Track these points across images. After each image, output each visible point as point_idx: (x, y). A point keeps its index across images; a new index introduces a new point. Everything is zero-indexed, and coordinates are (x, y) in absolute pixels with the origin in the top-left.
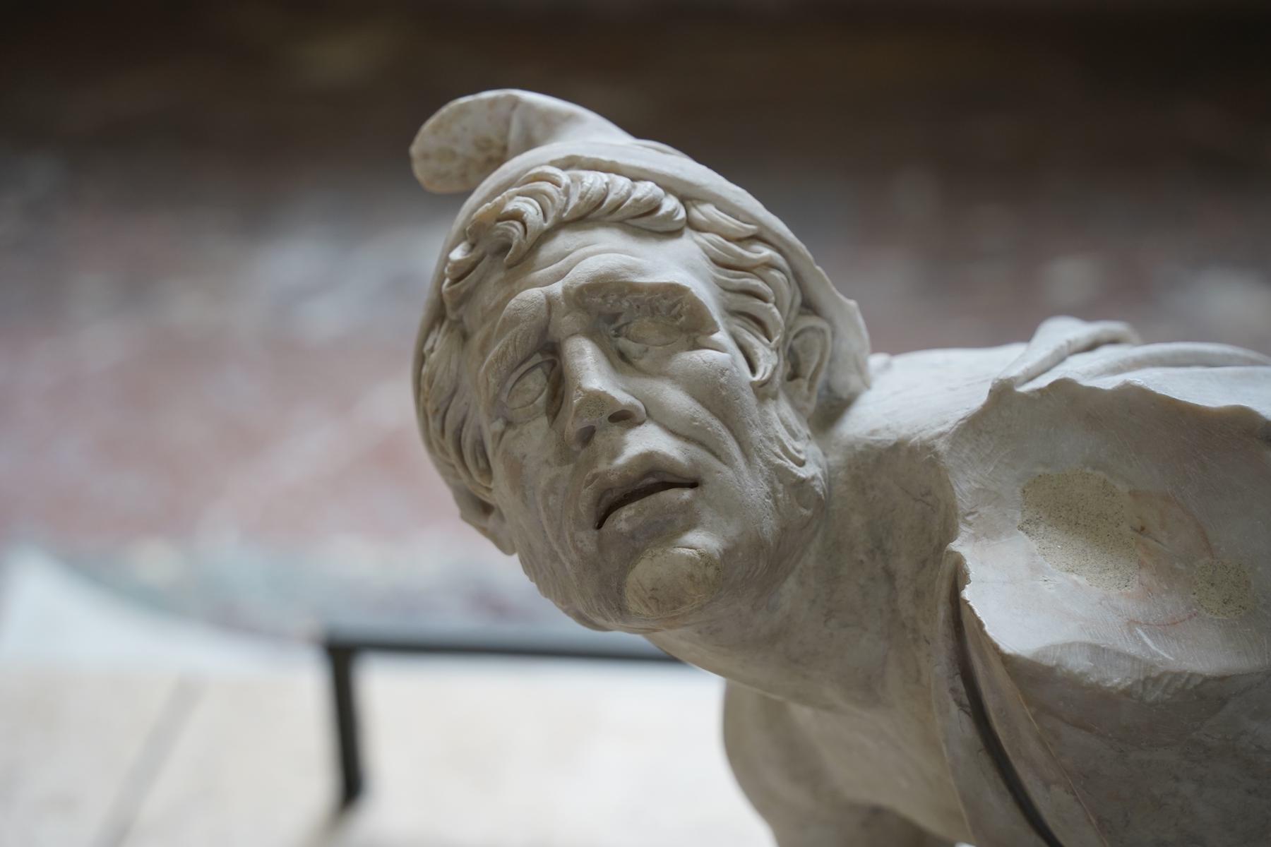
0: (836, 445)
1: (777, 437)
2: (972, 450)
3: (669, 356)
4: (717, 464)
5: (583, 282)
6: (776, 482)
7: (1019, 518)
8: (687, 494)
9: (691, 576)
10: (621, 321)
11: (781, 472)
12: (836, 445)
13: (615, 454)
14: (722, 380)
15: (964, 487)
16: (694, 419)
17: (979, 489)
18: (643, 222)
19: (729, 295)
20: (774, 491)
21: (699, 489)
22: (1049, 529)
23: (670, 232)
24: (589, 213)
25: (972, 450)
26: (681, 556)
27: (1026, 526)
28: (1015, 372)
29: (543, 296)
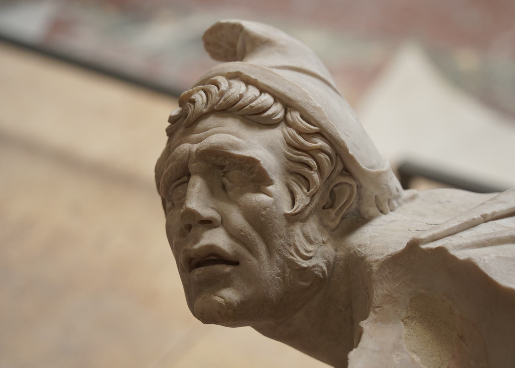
0: (344, 246)
1: (294, 244)
2: (390, 273)
3: (243, 192)
4: (249, 256)
5: (205, 148)
6: (286, 268)
7: (403, 314)
8: (228, 269)
9: (219, 312)
10: (225, 170)
11: (291, 264)
12: (344, 246)
13: (197, 241)
14: (264, 213)
15: (380, 292)
16: (242, 231)
17: (387, 295)
18: (254, 117)
19: (291, 164)
20: (284, 272)
21: (237, 267)
22: (418, 324)
23: (270, 124)
24: (228, 108)
25: (390, 273)
26: (216, 301)
27: (406, 320)
28: (424, 236)
29: (188, 148)
